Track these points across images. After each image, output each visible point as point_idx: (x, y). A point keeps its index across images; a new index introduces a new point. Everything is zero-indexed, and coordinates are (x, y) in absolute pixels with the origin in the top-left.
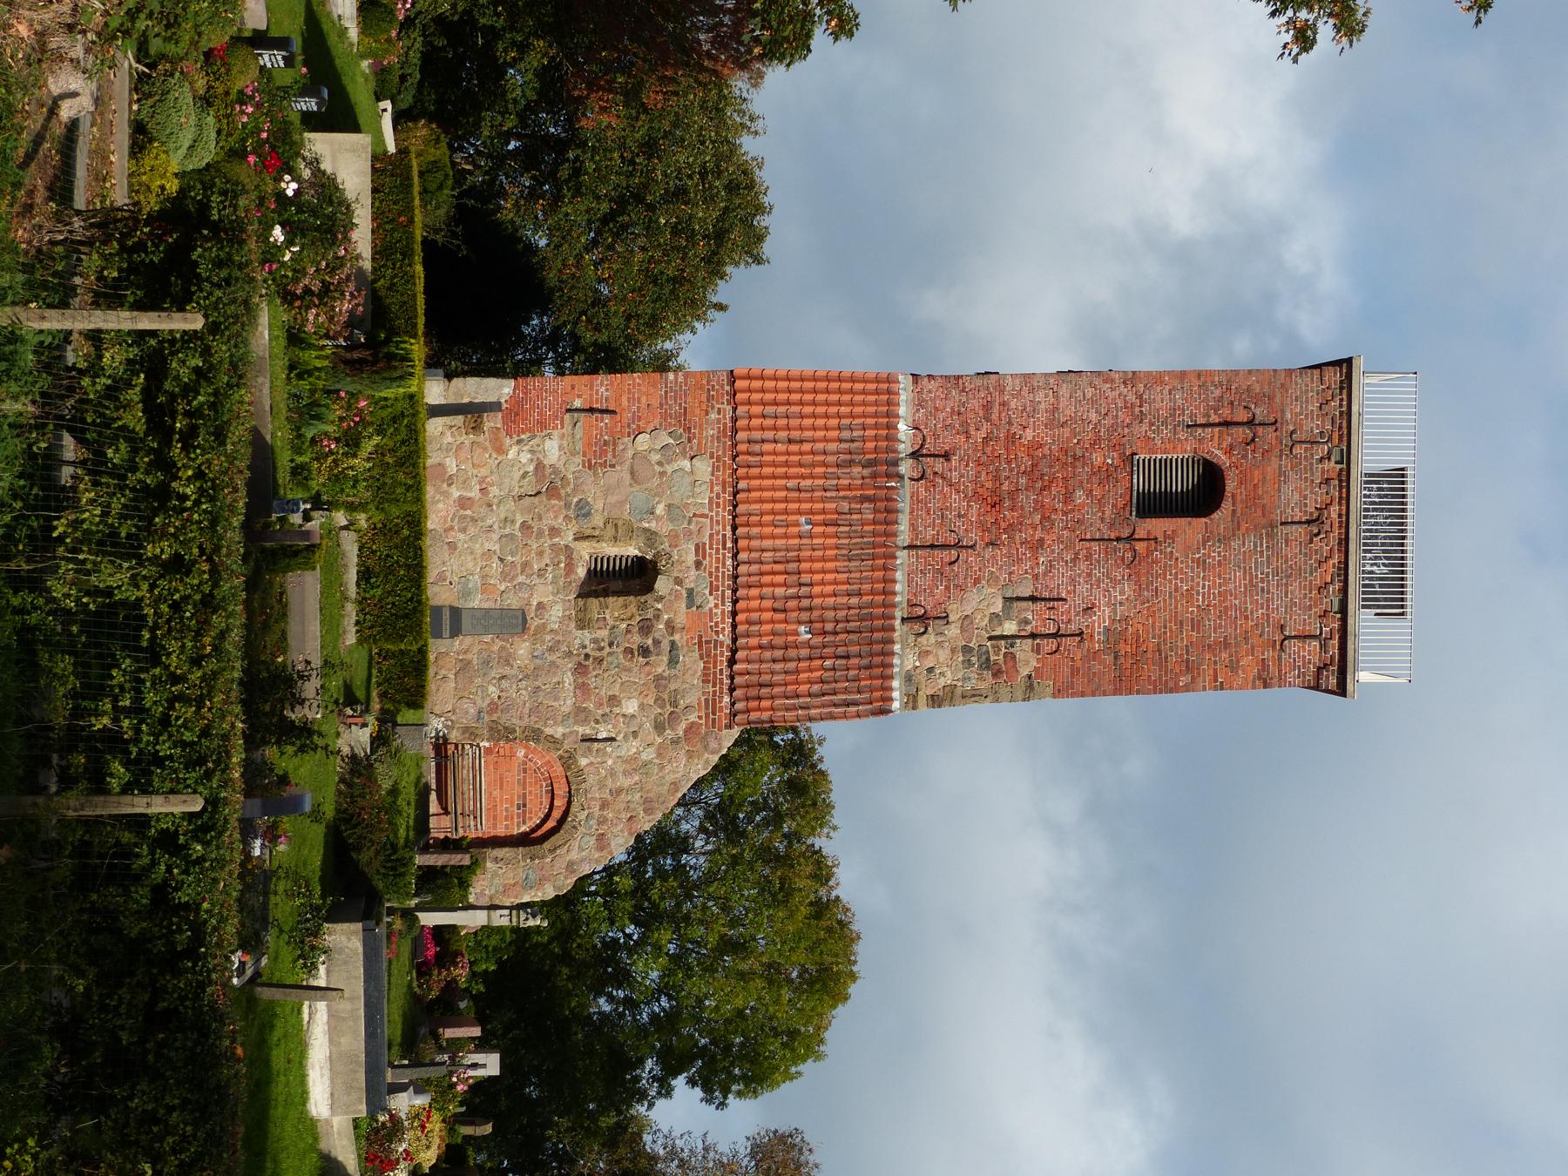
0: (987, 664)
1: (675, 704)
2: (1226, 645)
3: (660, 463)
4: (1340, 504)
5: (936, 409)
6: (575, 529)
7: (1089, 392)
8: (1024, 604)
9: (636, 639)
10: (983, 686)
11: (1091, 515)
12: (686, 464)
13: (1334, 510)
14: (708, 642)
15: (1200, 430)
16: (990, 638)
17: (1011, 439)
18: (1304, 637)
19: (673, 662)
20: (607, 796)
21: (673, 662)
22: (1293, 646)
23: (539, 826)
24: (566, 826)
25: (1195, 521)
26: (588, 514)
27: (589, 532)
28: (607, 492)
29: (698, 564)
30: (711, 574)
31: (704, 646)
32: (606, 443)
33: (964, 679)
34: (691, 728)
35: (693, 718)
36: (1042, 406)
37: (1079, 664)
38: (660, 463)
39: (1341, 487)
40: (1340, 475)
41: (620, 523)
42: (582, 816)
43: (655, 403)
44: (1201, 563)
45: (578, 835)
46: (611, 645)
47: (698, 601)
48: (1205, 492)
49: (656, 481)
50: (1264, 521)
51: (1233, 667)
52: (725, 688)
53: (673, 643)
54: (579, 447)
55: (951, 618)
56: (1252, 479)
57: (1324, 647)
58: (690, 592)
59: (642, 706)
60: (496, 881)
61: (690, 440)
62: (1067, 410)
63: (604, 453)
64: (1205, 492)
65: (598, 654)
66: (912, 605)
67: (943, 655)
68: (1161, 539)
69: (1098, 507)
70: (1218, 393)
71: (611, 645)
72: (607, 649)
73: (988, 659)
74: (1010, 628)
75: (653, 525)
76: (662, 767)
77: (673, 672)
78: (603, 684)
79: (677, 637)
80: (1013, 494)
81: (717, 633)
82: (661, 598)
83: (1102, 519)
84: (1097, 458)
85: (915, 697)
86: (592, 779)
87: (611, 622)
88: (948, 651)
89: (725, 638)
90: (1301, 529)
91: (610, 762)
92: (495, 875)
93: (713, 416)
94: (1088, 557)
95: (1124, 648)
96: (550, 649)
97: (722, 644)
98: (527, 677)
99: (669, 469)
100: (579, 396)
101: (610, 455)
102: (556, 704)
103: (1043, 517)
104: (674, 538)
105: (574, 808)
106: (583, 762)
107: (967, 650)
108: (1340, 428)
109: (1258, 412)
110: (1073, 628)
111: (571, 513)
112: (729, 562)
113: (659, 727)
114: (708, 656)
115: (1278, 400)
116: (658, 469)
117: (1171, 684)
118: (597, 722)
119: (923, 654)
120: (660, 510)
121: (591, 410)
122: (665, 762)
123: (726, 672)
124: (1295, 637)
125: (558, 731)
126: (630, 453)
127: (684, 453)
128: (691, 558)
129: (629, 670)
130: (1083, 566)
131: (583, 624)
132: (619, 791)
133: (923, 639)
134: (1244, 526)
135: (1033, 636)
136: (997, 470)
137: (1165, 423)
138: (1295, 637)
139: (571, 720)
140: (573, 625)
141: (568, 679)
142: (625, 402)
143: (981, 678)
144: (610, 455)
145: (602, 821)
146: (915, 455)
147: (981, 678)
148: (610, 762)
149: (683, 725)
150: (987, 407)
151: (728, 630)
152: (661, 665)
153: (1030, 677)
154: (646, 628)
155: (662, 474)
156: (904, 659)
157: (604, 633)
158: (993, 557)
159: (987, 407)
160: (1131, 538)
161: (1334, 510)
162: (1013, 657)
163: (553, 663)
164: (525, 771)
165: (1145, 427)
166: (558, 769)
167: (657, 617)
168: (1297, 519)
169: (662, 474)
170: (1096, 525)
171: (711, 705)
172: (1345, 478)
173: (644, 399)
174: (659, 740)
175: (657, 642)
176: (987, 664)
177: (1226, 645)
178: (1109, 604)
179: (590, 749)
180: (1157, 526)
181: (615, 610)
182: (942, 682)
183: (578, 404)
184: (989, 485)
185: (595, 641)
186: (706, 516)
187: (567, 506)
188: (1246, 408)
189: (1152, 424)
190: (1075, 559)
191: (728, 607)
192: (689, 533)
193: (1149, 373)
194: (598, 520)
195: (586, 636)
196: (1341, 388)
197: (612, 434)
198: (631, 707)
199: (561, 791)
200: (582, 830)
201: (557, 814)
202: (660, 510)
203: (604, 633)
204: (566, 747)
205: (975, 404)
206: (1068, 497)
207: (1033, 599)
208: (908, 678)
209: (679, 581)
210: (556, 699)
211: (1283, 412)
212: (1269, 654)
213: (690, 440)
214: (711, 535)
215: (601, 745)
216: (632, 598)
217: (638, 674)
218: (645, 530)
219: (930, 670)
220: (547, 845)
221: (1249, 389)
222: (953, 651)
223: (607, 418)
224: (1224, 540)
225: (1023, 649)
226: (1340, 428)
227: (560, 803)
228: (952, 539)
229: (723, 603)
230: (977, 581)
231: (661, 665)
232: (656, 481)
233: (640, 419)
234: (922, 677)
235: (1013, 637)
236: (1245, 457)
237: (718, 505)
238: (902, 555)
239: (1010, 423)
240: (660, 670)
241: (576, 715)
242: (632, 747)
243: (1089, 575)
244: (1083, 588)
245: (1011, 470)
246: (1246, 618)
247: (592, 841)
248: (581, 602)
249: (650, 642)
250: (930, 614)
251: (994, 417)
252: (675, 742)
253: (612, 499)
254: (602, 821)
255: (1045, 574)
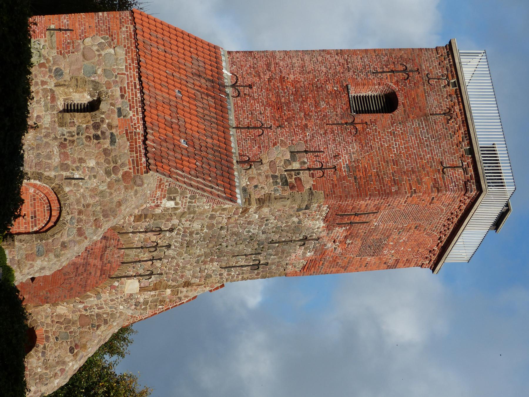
0: (285, 183)
1: (116, 162)
2: (414, 172)
3: (98, 51)
4: (459, 105)
5: (242, 66)
6: (55, 82)
7: (320, 59)
8: (302, 154)
9: (92, 132)
10: (286, 194)
11: (330, 112)
12: (112, 51)
13: (457, 108)
14: (130, 133)
15: (380, 75)
16: (286, 171)
17: (282, 79)
18: (454, 167)
19: (113, 141)
20: (81, 207)
21: (113, 141)
22: (449, 172)
23: (43, 227)
24: (59, 223)
25: (386, 115)
26: (62, 74)
27: (62, 83)
28: (71, 64)
29: (122, 96)
30: (129, 100)
31: (130, 135)
32: (68, 43)
33: (275, 190)
34: (125, 174)
35: (126, 169)
36: (297, 65)
37: (336, 182)
38: (98, 51)
39: (458, 97)
40: (456, 92)
41: (79, 78)
42: (69, 217)
43: (93, 25)
44: (393, 134)
45: (67, 228)
46: (78, 134)
47: (124, 113)
48: (389, 103)
49: (97, 59)
50: (421, 113)
51: (419, 182)
52: (143, 154)
53: (112, 134)
54: (55, 45)
55: (264, 162)
56: (411, 95)
57: (465, 171)
58: (119, 110)
59: (98, 163)
60: (21, 252)
61: (112, 40)
62: (310, 66)
63: (67, 47)
64: (389, 103)
65: (71, 138)
66: (240, 155)
67: (262, 178)
68: (369, 123)
69: (335, 111)
70: (386, 58)
71: (78, 134)
72: (76, 136)
73: (286, 181)
74: (296, 165)
75: (97, 78)
76: (111, 194)
77: (113, 147)
78: (75, 152)
79: (114, 131)
80: (288, 104)
81: (136, 128)
82: (103, 113)
83: (337, 115)
84: (329, 87)
85: (249, 200)
86: (72, 199)
87: (77, 124)
88: (264, 177)
89: (140, 130)
90: (442, 117)
91: (82, 190)
92: (20, 248)
93: (124, 29)
94: (332, 132)
95: (360, 174)
96: (45, 136)
97: (139, 134)
98: (33, 148)
99: (103, 53)
100: (53, 24)
101: (71, 48)
102: (49, 161)
103: (305, 114)
104: (108, 85)
105: (64, 213)
106: (67, 189)
107: (274, 177)
108: (452, 72)
109: (408, 66)
110: (330, 165)
111: (52, 74)
112: (139, 95)
113: (108, 173)
114: (132, 138)
115: (417, 61)
116: (97, 53)
117: (388, 191)
118: (73, 170)
119: (251, 179)
120: (99, 72)
121: (60, 30)
122: (113, 191)
123: (142, 147)
124: (449, 167)
125: (52, 174)
126: (82, 47)
127: (110, 46)
128: (118, 93)
129: (89, 146)
130: (330, 136)
131: (61, 125)
132: (88, 206)
133: (250, 171)
134: (411, 116)
135: (309, 169)
136: (278, 92)
137: (361, 71)
138: (449, 167)
139: (59, 168)
140: (57, 125)
141: (56, 150)
142: (77, 25)
143: (284, 190)
144: (71, 48)
145: (79, 221)
146: (234, 86)
147: (284, 190)
148: (82, 190)
149: (121, 173)
150: (268, 65)
151: (141, 127)
152: (106, 144)
153: (310, 189)
154: (96, 126)
155: (100, 55)
156: (241, 180)
157: (74, 129)
158: (282, 133)
159: (268, 65)
160: (353, 123)
161: (457, 108)
162: (300, 179)
163: (47, 142)
164: (34, 199)
165: (351, 73)
166: (53, 196)
167: (102, 121)
168: (438, 112)
169: (100, 55)
170: (334, 116)
171: (136, 163)
172: (471, 151)
173: (87, 24)
174: (109, 180)
175: (103, 133)
176: (285, 183)
177: (414, 172)
178: (347, 153)
179: (70, 184)
180: (367, 117)
181: (80, 120)
182: (263, 192)
183: (52, 27)
184: (274, 99)
185: (69, 132)
186: (125, 74)
187: (50, 71)
188: (403, 63)
189: (354, 72)
190: (325, 133)
191: (140, 116)
192: (116, 82)
193: (349, 51)
194: (67, 77)
195: (65, 130)
196: (448, 55)
197: (71, 39)
198: (92, 163)
199: (55, 206)
200: (68, 225)
201: (54, 219)
202: (99, 72)
203: (74, 129)
204: (57, 182)
205: (260, 63)
206: (317, 105)
207: (306, 152)
208: (244, 190)
209: (112, 105)
210: (50, 158)
211: (420, 65)
212: (437, 176)
213: (112, 40)
214: (128, 83)
215: (76, 181)
216: (88, 113)
217: (92, 147)
218: (93, 81)
219: (256, 186)
220: (49, 233)
221: (401, 57)
222: (267, 177)
223: (68, 33)
224: (403, 123)
225: (304, 176)
226: (452, 72)
227: (55, 213)
228: (259, 124)
229: (137, 114)
230: (275, 144)
231: (106, 144)
232: (97, 59)
233: (85, 32)
234: (251, 190)
235: (297, 170)
236: (405, 85)
237: (130, 69)
238: (232, 132)
239: (281, 72)
240: (106, 146)
241: (61, 167)
242: (94, 182)
243: (334, 140)
244: (332, 146)
245: (285, 93)
246: (421, 159)
247: (75, 231)
248: (60, 115)
249: (99, 133)
250: (251, 159)
251: (273, 69)
252: (118, 181)
253: (73, 67)
254: (79, 221)
255: (310, 140)
